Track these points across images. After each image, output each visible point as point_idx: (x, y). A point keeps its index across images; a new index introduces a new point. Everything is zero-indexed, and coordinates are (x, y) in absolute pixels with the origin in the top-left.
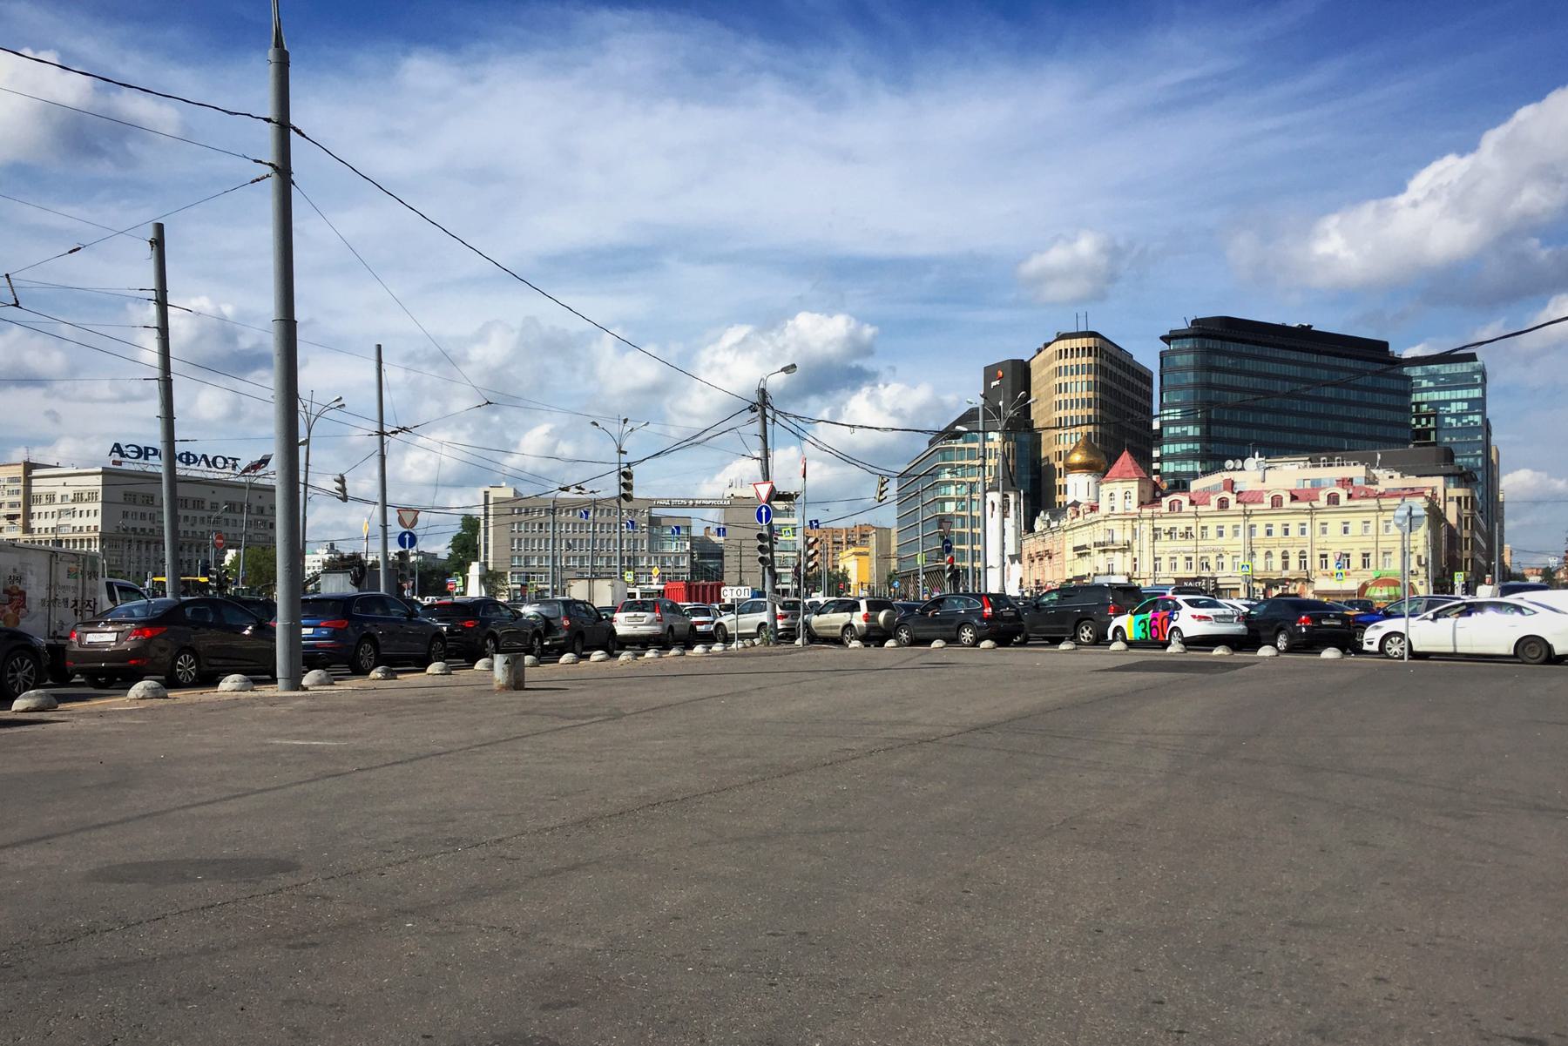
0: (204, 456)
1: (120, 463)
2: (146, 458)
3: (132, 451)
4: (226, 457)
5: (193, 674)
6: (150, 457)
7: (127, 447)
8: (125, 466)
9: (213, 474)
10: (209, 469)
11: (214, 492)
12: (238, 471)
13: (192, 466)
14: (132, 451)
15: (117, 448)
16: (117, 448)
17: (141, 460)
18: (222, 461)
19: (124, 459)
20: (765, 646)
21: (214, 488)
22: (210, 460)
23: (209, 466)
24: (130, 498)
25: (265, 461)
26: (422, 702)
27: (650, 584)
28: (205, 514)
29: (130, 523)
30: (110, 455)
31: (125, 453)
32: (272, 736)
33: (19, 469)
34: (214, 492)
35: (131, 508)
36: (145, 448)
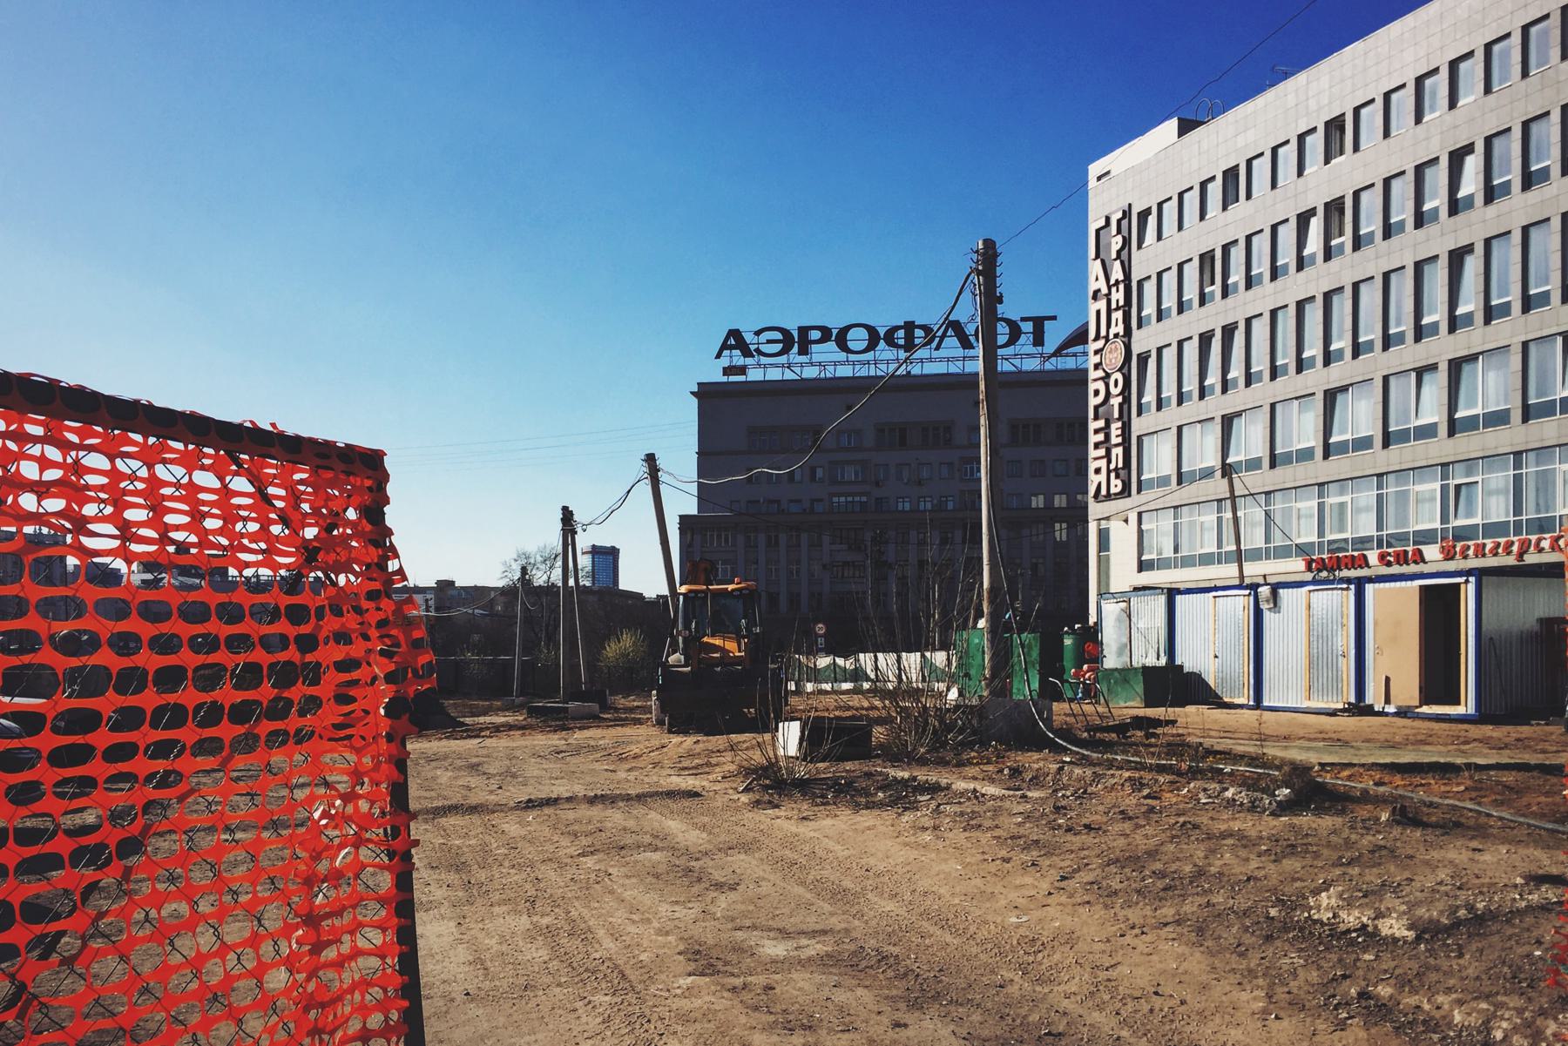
1: (742, 370)
2: (804, 351)
3: (769, 342)
4: (1015, 317)
7: (758, 333)
8: (754, 375)
12: (1051, 345)
13: (922, 353)
14: (769, 342)
15: (735, 340)
16: (735, 340)
19: (749, 361)
25: (1508, 35)
26: (632, 710)
30: (718, 356)
31: (753, 347)
32: (1002, 798)
33: (1502, 511)
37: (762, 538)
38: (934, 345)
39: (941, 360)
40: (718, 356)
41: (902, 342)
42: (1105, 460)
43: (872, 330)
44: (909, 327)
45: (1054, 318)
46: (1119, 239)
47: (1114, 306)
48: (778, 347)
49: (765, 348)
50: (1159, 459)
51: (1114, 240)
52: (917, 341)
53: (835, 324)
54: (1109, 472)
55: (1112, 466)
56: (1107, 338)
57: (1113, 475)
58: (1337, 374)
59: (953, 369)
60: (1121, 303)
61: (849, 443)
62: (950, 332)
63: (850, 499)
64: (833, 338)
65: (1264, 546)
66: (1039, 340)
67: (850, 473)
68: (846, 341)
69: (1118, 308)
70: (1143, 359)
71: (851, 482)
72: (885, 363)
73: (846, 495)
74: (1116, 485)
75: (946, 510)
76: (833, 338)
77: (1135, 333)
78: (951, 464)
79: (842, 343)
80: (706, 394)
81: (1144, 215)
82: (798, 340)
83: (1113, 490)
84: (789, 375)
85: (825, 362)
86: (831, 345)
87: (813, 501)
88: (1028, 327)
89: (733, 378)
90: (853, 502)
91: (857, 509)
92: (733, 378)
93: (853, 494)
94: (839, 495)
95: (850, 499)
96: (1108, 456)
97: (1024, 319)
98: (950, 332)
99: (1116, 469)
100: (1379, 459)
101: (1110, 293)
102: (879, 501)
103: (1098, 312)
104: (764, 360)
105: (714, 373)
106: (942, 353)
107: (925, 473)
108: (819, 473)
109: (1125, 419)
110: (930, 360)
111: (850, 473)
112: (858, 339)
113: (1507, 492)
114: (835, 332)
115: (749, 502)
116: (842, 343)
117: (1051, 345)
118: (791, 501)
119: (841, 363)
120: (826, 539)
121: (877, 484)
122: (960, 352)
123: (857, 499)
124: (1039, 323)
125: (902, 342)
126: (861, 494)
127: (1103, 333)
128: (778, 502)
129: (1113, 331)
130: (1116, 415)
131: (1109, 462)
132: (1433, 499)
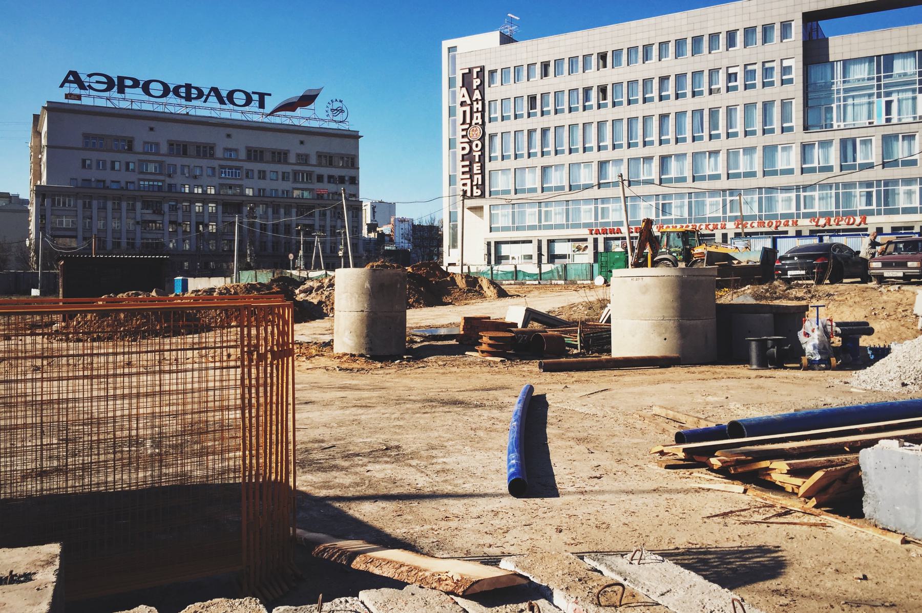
0: (215, 90)
1: (79, 97)
2: (121, 90)
3: (98, 82)
4: (250, 91)
5: (567, 348)
6: (127, 90)
7: (90, 76)
8: (86, 101)
9: (227, 113)
10: (223, 107)
11: (302, 143)
12: (269, 108)
13: (194, 103)
14: (98, 82)
16: (74, 77)
17: (114, 93)
18: (243, 96)
19: (83, 92)
20: (391, 207)
21: (153, 124)
22: (224, 94)
23: (221, 101)
24: (92, 141)
27: (665, 196)
28: (288, 169)
29: (94, 174)
30: (62, 86)
31: (86, 84)
34: (151, 129)
35: (93, 156)
36: (119, 77)
37: (80, 202)
38: (203, 99)
39: (206, 108)
40: (62, 86)
41: (183, 95)
42: (470, 180)
43: (165, 86)
44: (188, 87)
45: (270, 95)
46: (479, 81)
47: (475, 110)
48: (104, 86)
49: (93, 85)
50: (502, 182)
51: (475, 81)
52: (193, 96)
53: (143, 78)
54: (472, 186)
55: (475, 183)
56: (470, 124)
57: (475, 188)
58: (604, 155)
59: (214, 114)
60: (480, 109)
61: (151, 150)
62: (212, 93)
63: (151, 183)
64: (141, 86)
65: (795, 212)
66: (262, 105)
67: (151, 168)
68: (164, 90)
69: (478, 111)
70: (491, 137)
71: (151, 173)
72: (174, 105)
73: (149, 180)
74: (476, 192)
75: (293, 198)
76: (141, 86)
77: (487, 124)
78: (213, 169)
79: (146, 88)
80: (53, 109)
81: (492, 72)
82: (119, 84)
83: (475, 194)
84: (110, 105)
85: (134, 100)
86: (139, 90)
87: (127, 183)
88: (255, 97)
89: (71, 102)
90: (153, 185)
91: (156, 189)
92: (71, 102)
93: (153, 181)
94: (144, 180)
95: (151, 183)
96: (471, 178)
97: (254, 93)
98: (212, 93)
99: (477, 185)
100: (595, 193)
101: (472, 104)
102: (170, 185)
103: (465, 112)
104: (92, 92)
105: (59, 96)
106: (207, 104)
107: (198, 172)
108: (131, 166)
109: (482, 161)
110: (199, 107)
111: (151, 168)
112: (156, 89)
113: (563, 213)
114: (142, 83)
115: (83, 180)
116: (146, 88)
117: (269, 108)
118: (113, 182)
119: (144, 102)
120: (139, 205)
121: (169, 176)
122: (218, 105)
123: (155, 183)
124: (262, 96)
125: (183, 95)
126: (158, 181)
127: (468, 121)
128: (104, 181)
129: (474, 121)
130: (477, 160)
131: (472, 181)
132: (535, 214)
